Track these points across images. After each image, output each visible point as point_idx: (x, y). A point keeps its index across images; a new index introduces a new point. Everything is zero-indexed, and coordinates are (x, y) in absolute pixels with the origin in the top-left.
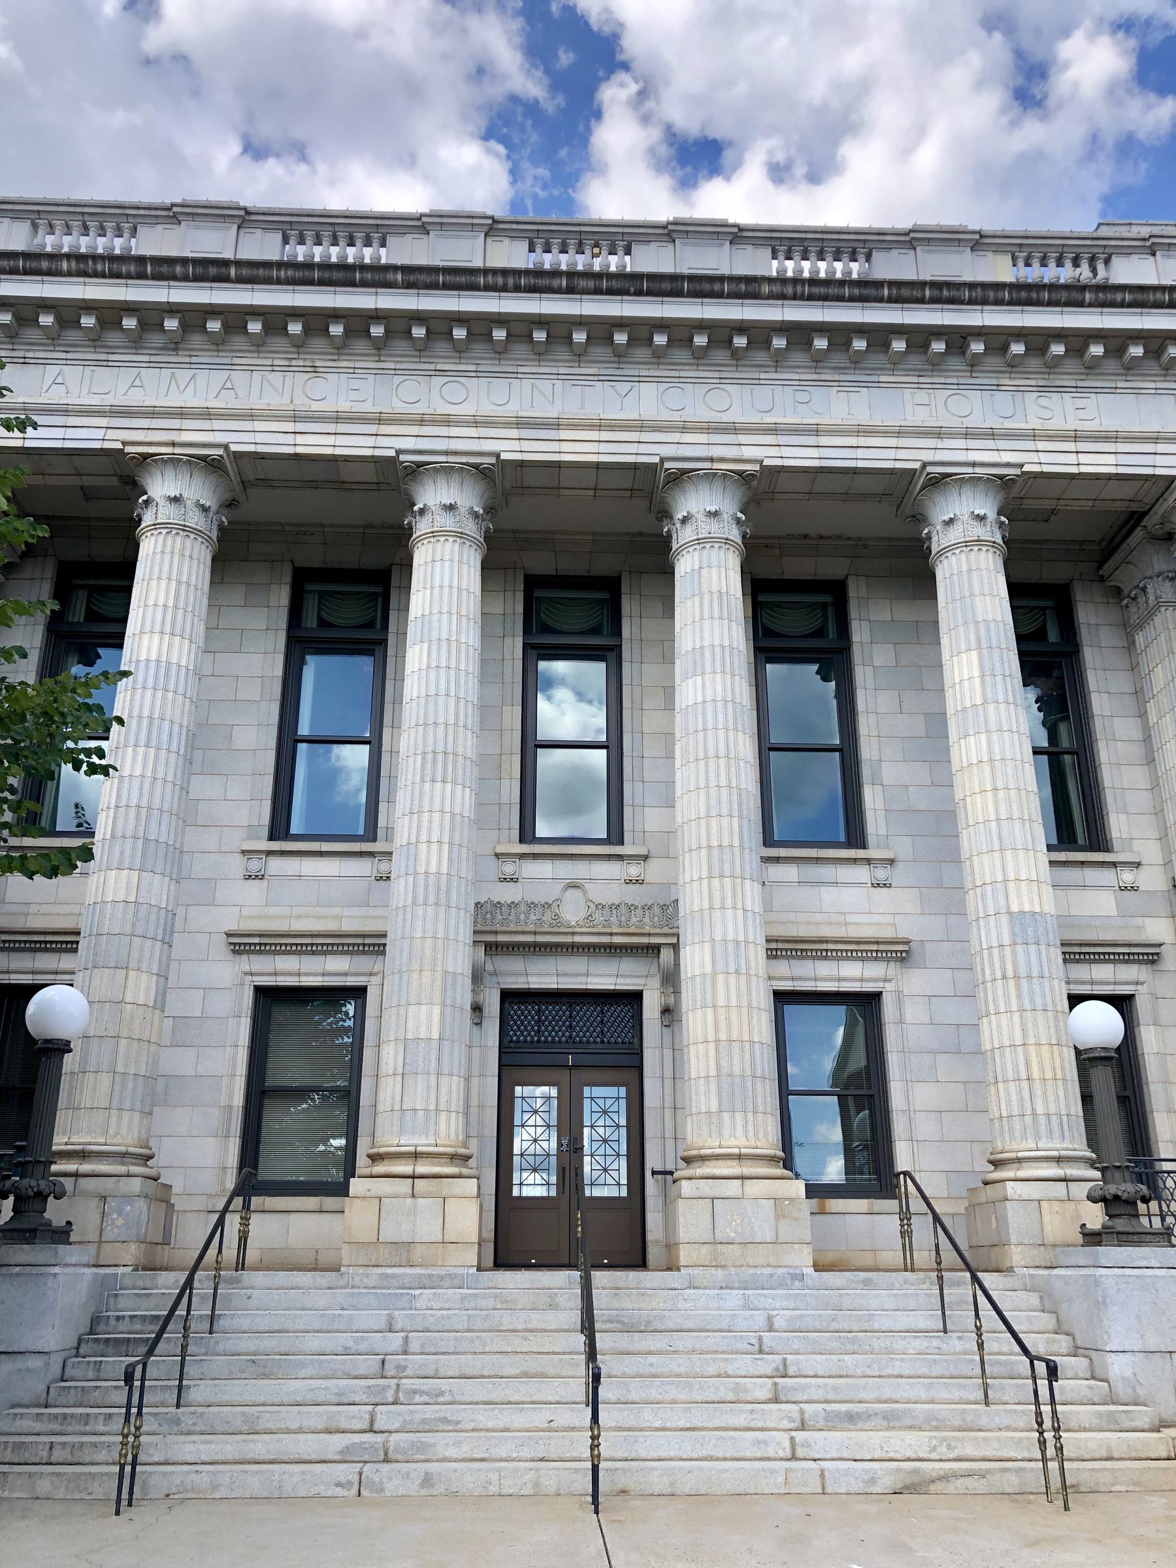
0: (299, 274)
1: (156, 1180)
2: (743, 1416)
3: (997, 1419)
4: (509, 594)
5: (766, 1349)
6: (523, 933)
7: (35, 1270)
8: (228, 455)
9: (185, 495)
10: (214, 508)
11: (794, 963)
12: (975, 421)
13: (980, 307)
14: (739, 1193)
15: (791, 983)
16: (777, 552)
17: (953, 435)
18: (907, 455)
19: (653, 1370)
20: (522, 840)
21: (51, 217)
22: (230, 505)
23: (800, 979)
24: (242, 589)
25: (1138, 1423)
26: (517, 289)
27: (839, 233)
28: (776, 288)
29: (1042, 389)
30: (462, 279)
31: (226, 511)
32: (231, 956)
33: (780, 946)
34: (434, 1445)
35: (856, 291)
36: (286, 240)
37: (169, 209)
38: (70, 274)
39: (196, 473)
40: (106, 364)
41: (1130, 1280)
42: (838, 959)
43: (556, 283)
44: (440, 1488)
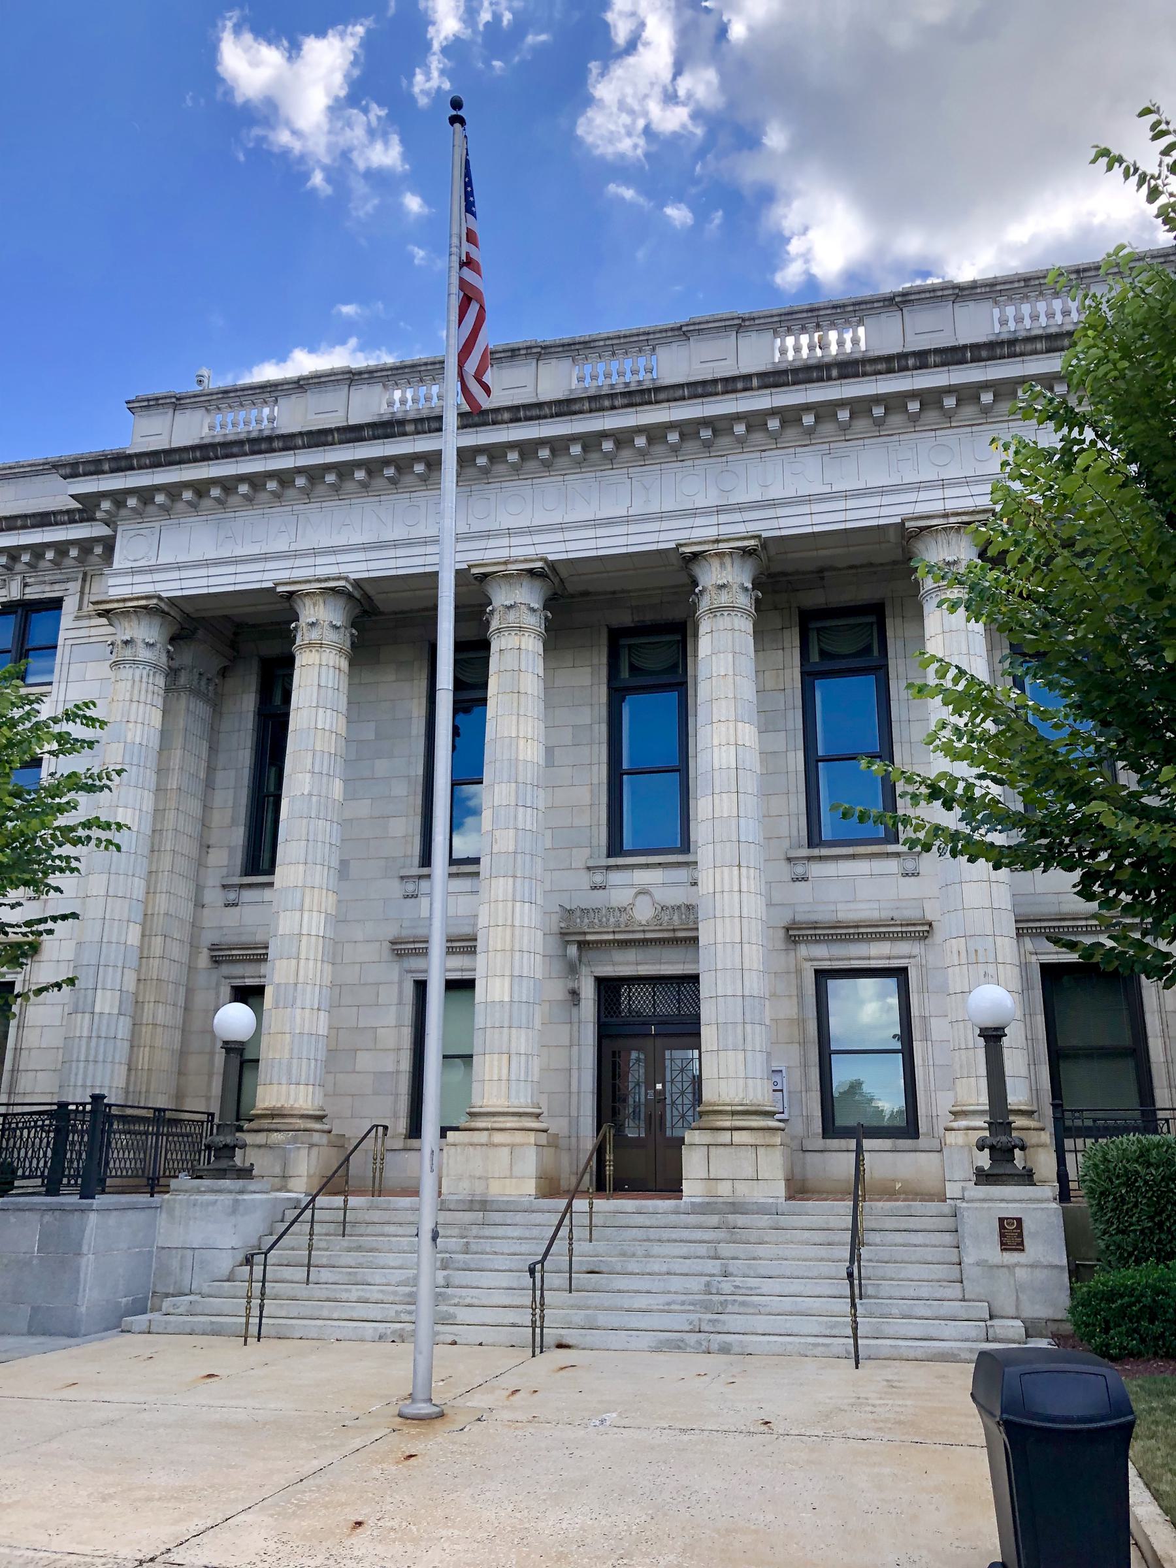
1: (545, 1131)
14: (728, 1141)
20: (810, 845)
32: (396, 958)
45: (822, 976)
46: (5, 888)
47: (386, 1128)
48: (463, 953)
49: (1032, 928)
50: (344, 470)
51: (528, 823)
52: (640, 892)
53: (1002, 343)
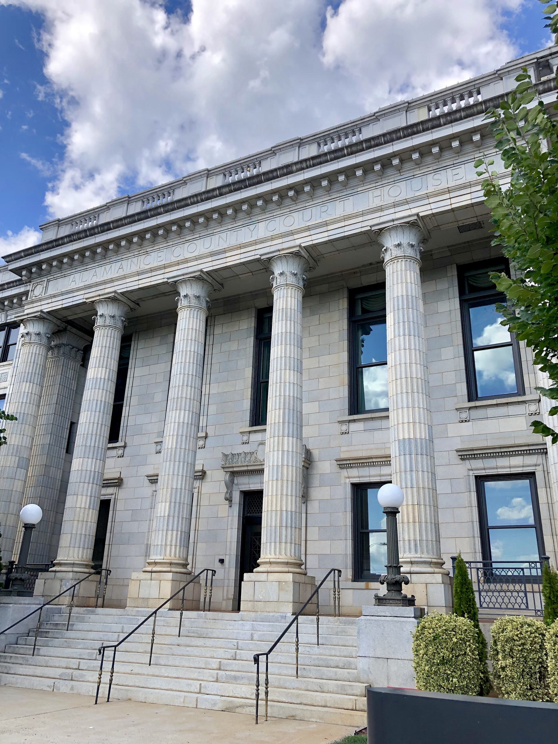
0: (131, 220)
2: (196, 674)
3: (293, 684)
4: (250, 319)
5: (240, 648)
6: (242, 466)
7: (6, 605)
8: (419, 218)
9: (402, 242)
10: (299, 273)
11: (360, 469)
12: (283, 229)
13: (391, 143)
15: (508, 470)
16: (359, 274)
17: (388, 208)
18: (79, 298)
19: (188, 653)
20: (470, 400)
21: (75, 220)
22: (424, 241)
23: (362, 477)
24: (159, 338)
25: (355, 692)
26: (202, 201)
27: (432, 96)
28: (299, 166)
29: (436, 171)
30: (183, 203)
31: (422, 245)
33: (351, 462)
34: (85, 675)
35: (333, 156)
36: (319, 145)
37: (374, 115)
38: (68, 243)
39: (109, 304)
40: (86, 270)
41: (372, 622)
42: (381, 466)
43: (215, 193)
44: (75, 692)
45: (480, 480)
47: (340, 571)
49: (488, 453)
50: (349, 172)
51: (27, 444)
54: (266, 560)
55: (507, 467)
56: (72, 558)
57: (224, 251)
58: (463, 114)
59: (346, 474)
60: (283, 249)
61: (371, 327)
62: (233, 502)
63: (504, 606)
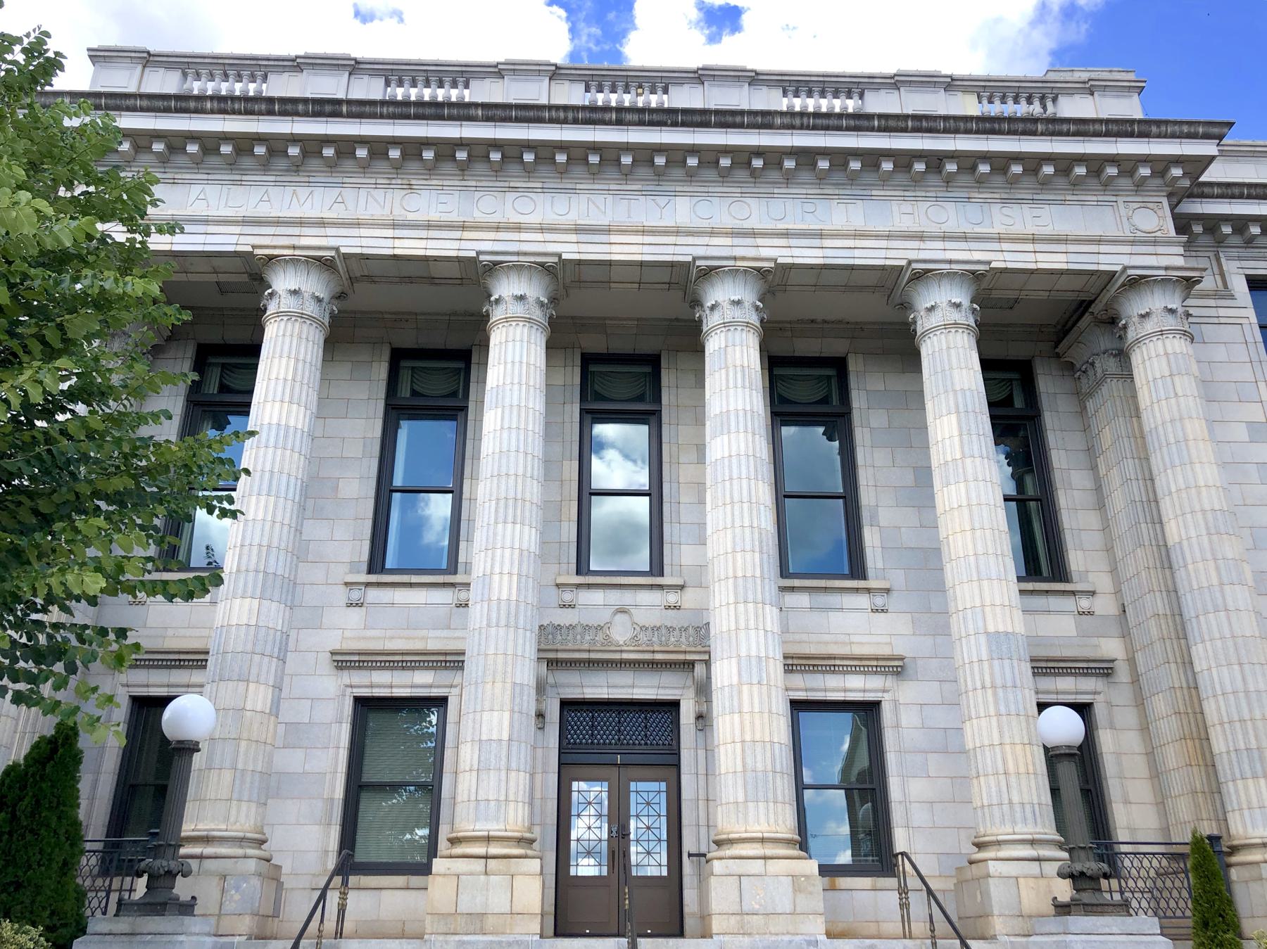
0: (398, 110)
1: (268, 861)
7: (165, 938)
9: (303, 289)
17: (933, 238)
20: (578, 573)
28: (787, 120)
29: (1005, 201)
32: (335, 671)
33: (796, 662)
36: (388, 84)
38: (212, 112)
40: (239, 183)
42: (845, 673)
43: (607, 116)
46: (6, 568)
48: (1096, 675)
52: (622, 617)
53: (1005, 119)
54: (754, 835)
55: (366, 687)
56: (238, 826)
57: (608, 231)
58: (1073, 128)
59: (348, 682)
60: (743, 259)
61: (231, 418)
62: (547, 719)
63: (1179, 913)
